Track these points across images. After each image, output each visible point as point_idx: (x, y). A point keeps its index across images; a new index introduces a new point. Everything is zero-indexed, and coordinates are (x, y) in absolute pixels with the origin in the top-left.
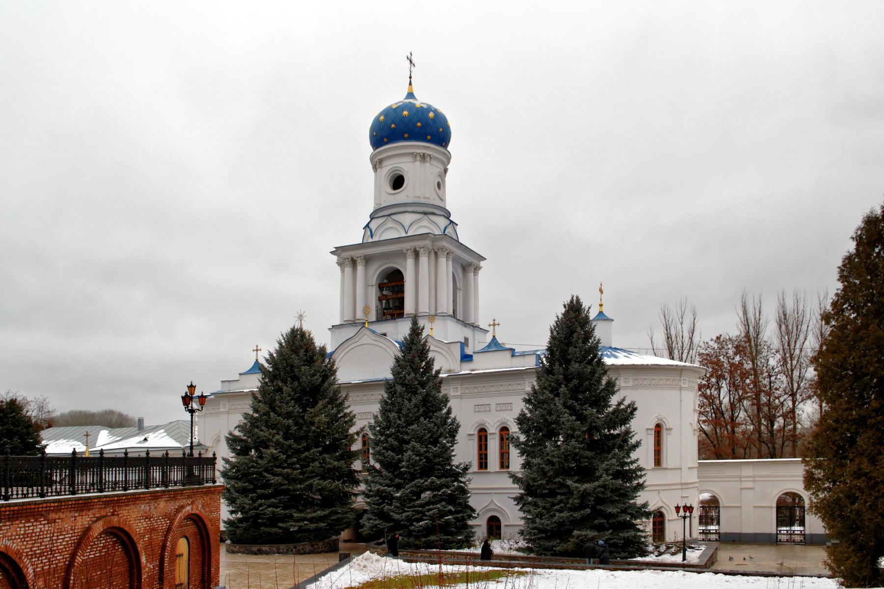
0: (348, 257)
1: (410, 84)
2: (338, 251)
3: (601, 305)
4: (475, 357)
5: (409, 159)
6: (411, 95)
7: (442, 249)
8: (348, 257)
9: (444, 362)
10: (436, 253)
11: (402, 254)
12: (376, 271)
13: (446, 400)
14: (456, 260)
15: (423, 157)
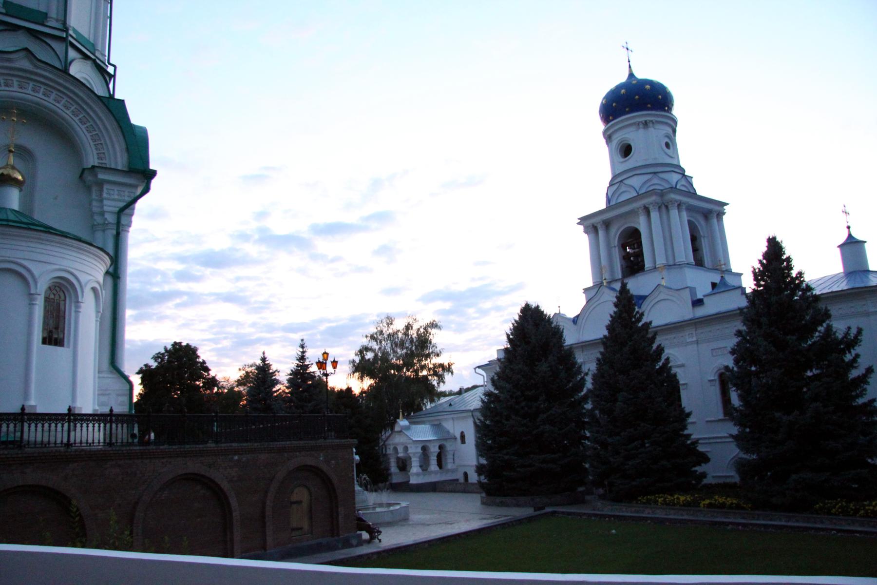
0: (593, 224)
1: (630, 67)
2: (583, 220)
3: (848, 227)
4: (705, 300)
5: (633, 129)
6: (631, 75)
7: (672, 201)
8: (593, 224)
9: (656, 315)
10: (667, 207)
11: (633, 213)
12: (616, 231)
13: (660, 350)
14: (690, 209)
15: (646, 124)
